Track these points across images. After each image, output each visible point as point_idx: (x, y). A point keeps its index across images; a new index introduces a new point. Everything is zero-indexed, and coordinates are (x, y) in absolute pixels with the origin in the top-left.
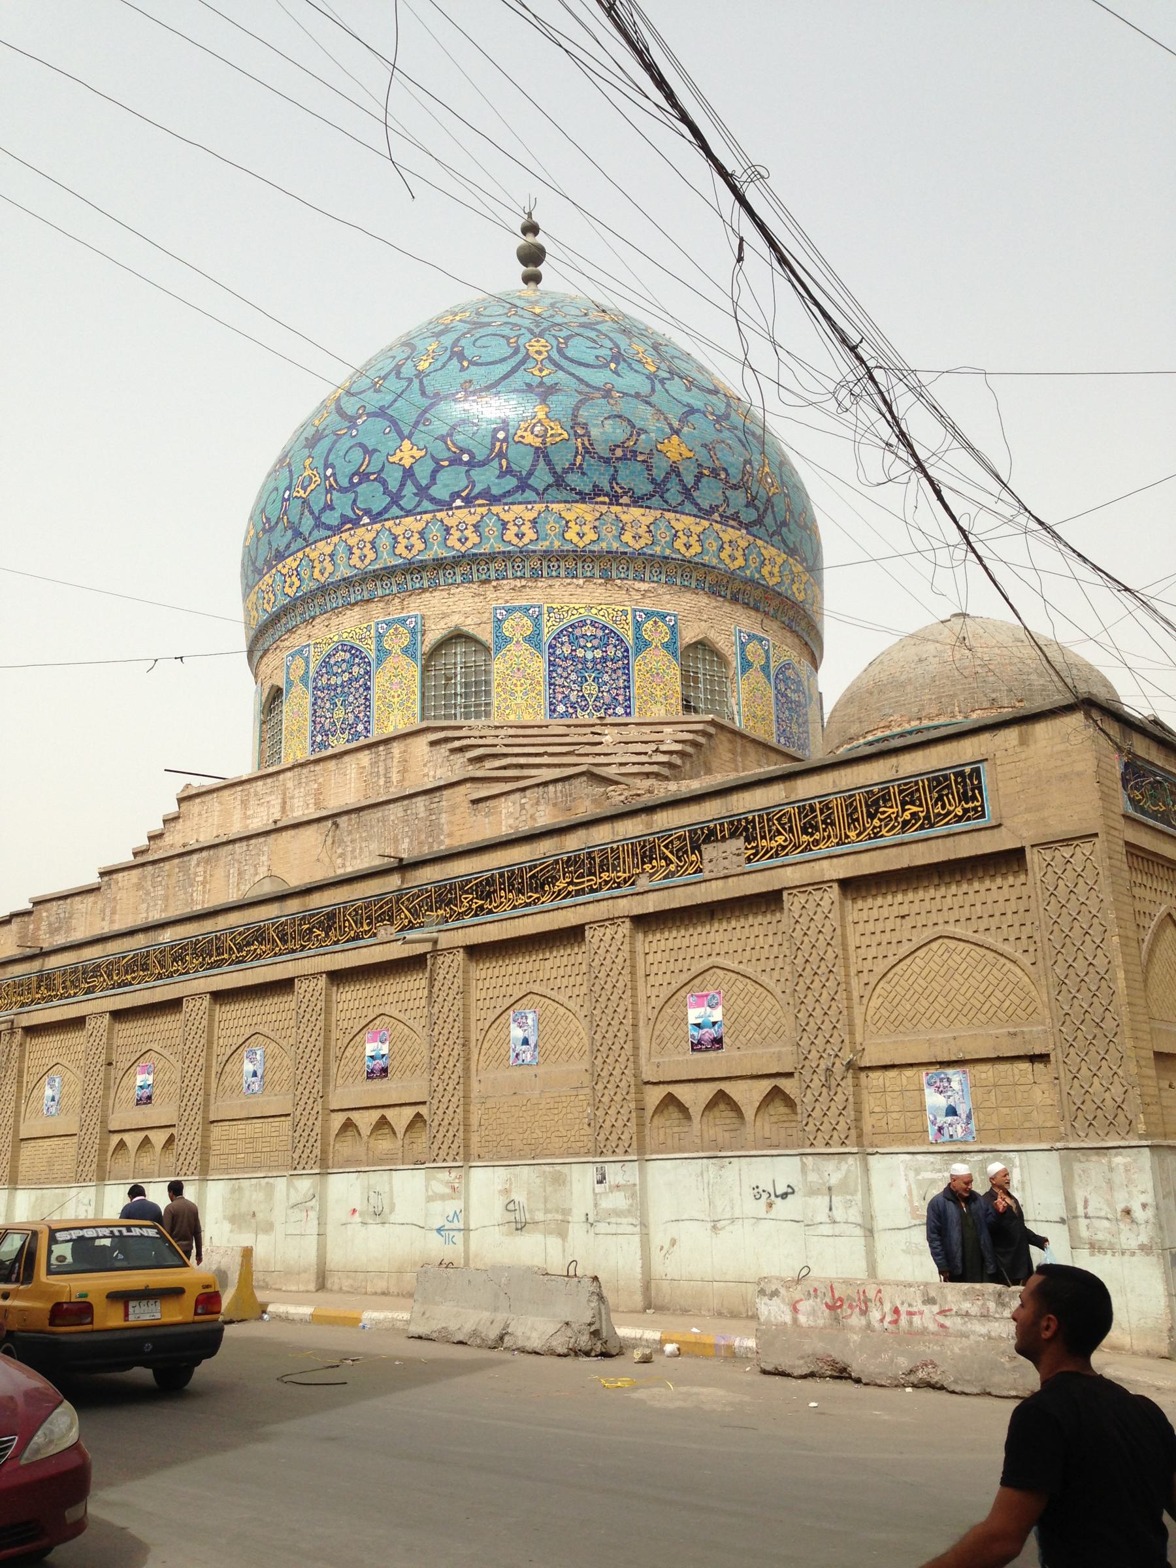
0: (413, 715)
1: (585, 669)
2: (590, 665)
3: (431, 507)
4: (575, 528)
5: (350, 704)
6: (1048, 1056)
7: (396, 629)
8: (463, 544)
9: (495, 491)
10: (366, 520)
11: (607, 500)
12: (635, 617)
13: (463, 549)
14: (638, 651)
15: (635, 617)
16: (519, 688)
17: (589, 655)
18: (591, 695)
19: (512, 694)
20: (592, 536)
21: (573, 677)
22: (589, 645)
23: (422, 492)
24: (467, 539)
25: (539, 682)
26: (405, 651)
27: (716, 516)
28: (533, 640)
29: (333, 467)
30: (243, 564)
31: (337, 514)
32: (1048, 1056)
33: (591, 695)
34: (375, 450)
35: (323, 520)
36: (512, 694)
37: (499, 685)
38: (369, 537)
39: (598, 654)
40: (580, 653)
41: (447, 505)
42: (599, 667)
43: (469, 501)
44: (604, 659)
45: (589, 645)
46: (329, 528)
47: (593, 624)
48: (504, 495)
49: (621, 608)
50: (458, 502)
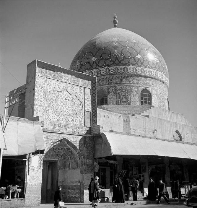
3: (98, 67)
4: (120, 70)
6: (176, 131)
9: (109, 64)
10: (87, 70)
11: (128, 65)
20: (114, 72)
23: (97, 65)
27: (147, 67)
29: (82, 61)
30: (80, 50)
31: (82, 69)
32: (176, 131)
34: (89, 59)
38: (105, 69)
41: (101, 67)
43: (105, 67)
46: (100, 66)
48: (111, 65)
50: (103, 67)
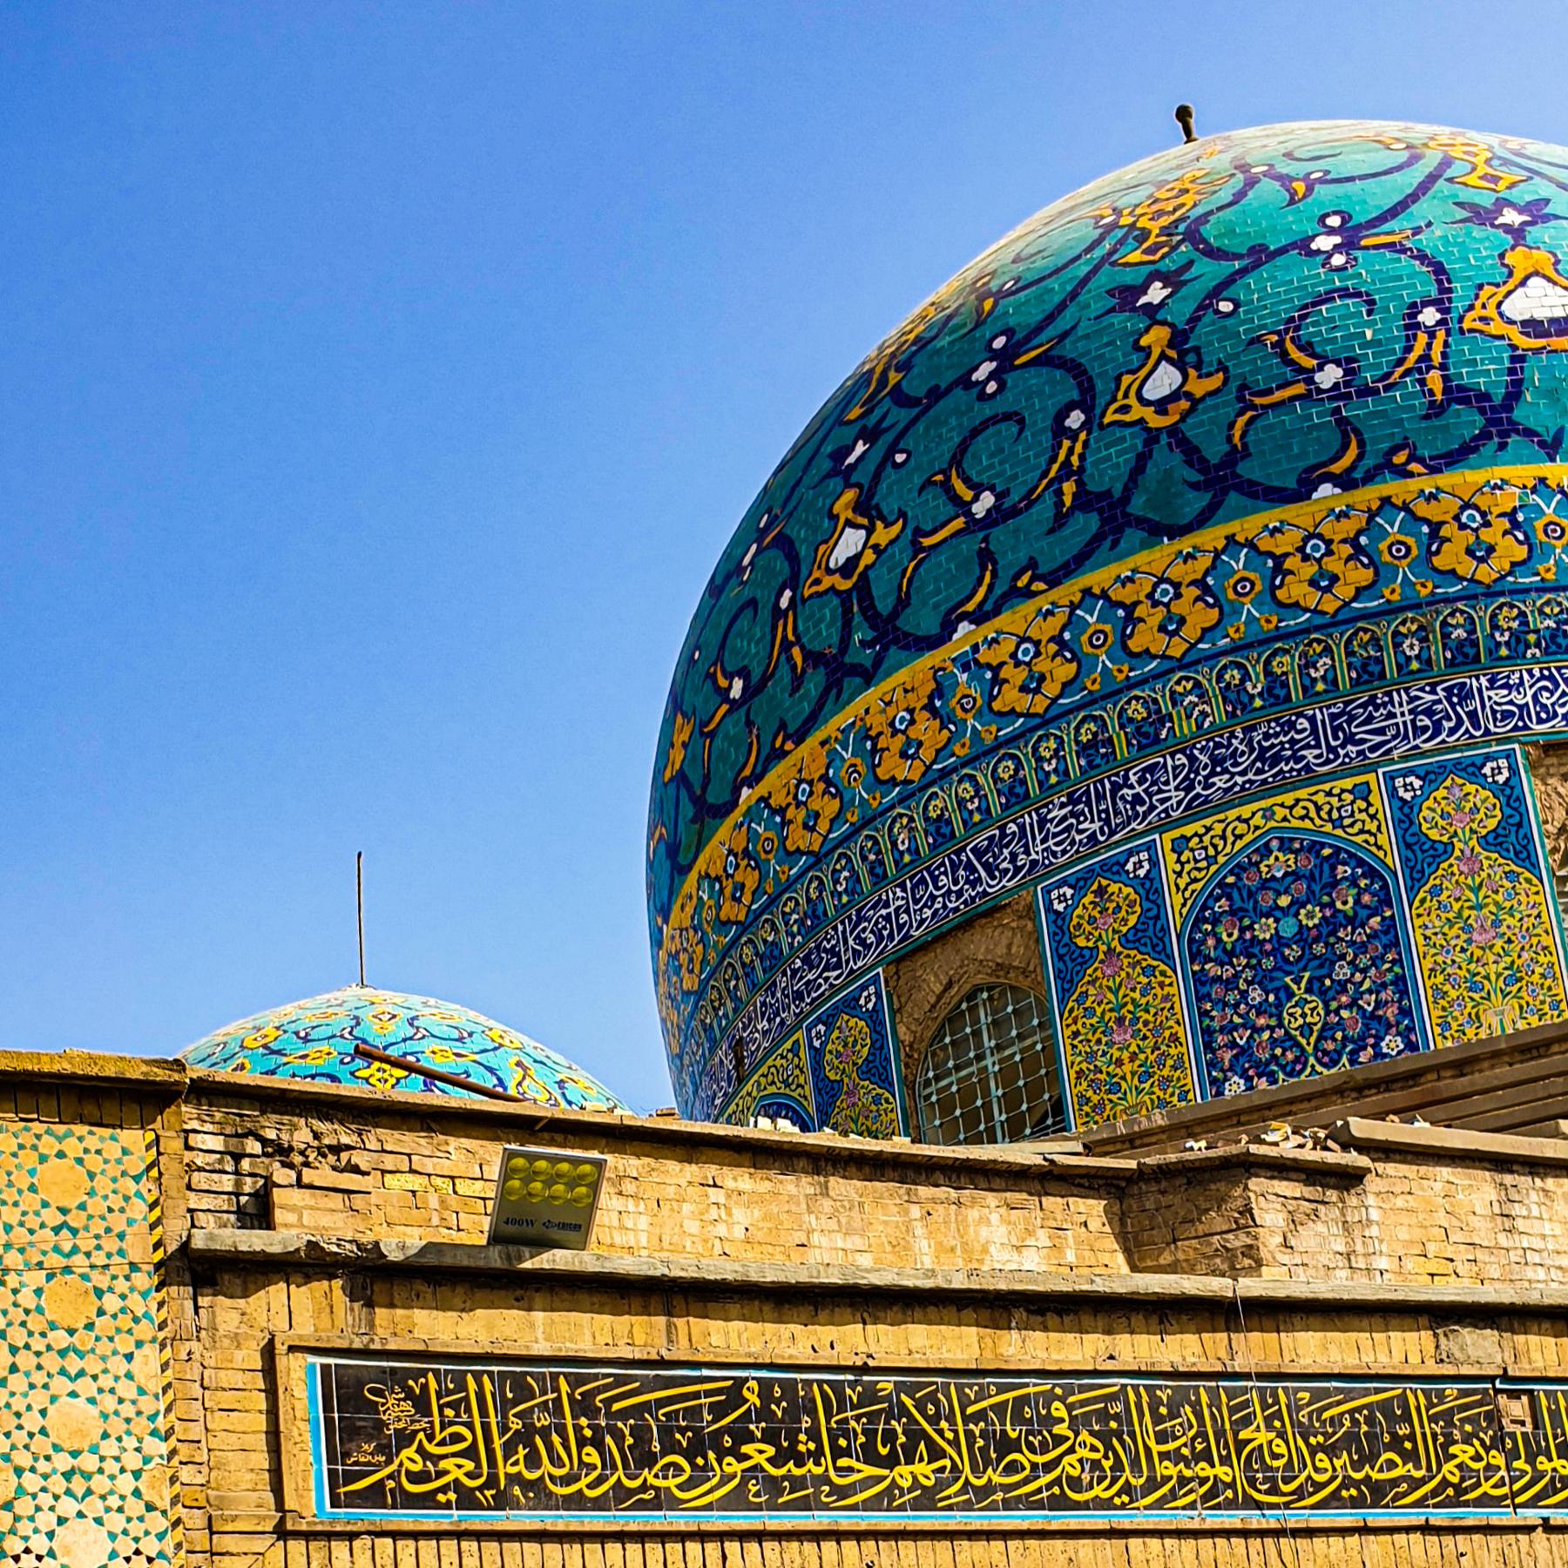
0: (1439, 993)
1: (1284, 965)
2: (1292, 953)
5: (1342, 987)
7: (1101, 891)
8: (812, 829)
12: (1393, 792)
13: (1330, 605)
14: (1416, 878)
15: (1393, 792)
16: (1127, 1068)
17: (1288, 928)
18: (1306, 1029)
19: (1114, 1088)
21: (1256, 995)
22: (1284, 901)
24: (1334, 579)
25: (1174, 1038)
26: (1133, 939)
28: (1149, 936)
33: (1306, 1029)
35: (1480, 421)
36: (1114, 1088)
37: (1080, 1074)
39: (1311, 917)
40: (1264, 930)
42: (1319, 949)
44: (1332, 923)
45: (1284, 901)
47: (1285, 845)
49: (1348, 783)
